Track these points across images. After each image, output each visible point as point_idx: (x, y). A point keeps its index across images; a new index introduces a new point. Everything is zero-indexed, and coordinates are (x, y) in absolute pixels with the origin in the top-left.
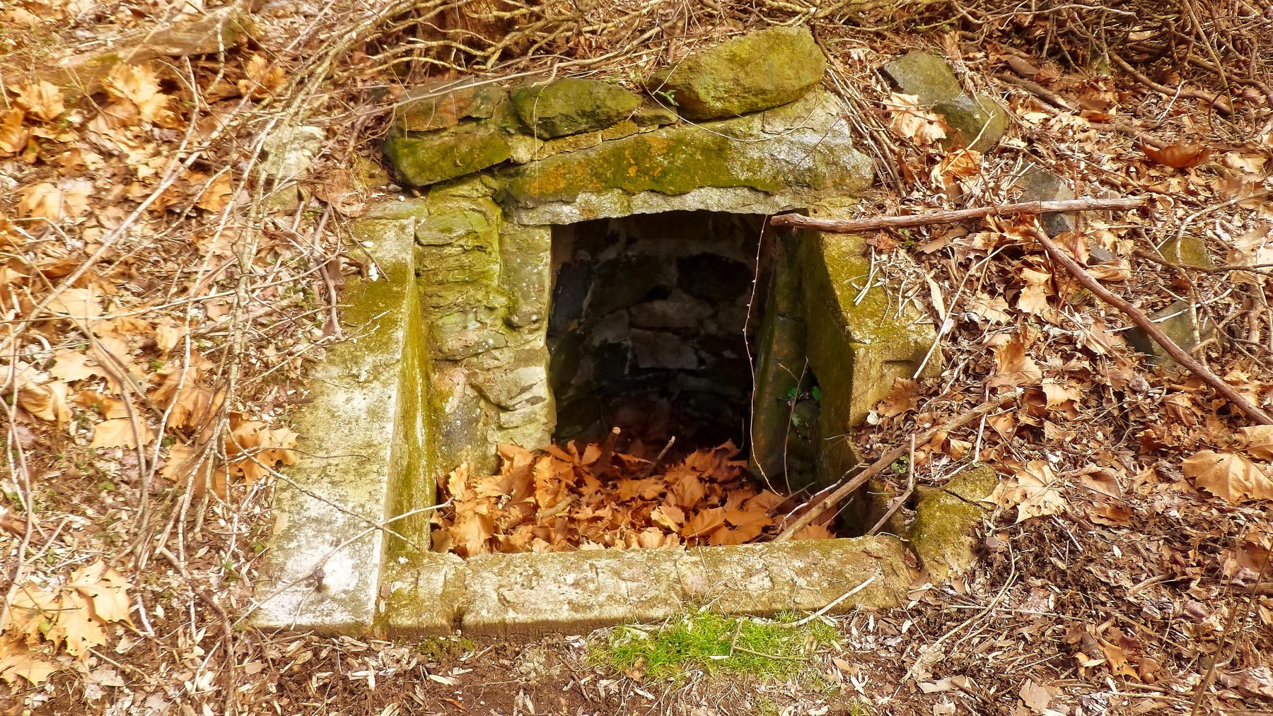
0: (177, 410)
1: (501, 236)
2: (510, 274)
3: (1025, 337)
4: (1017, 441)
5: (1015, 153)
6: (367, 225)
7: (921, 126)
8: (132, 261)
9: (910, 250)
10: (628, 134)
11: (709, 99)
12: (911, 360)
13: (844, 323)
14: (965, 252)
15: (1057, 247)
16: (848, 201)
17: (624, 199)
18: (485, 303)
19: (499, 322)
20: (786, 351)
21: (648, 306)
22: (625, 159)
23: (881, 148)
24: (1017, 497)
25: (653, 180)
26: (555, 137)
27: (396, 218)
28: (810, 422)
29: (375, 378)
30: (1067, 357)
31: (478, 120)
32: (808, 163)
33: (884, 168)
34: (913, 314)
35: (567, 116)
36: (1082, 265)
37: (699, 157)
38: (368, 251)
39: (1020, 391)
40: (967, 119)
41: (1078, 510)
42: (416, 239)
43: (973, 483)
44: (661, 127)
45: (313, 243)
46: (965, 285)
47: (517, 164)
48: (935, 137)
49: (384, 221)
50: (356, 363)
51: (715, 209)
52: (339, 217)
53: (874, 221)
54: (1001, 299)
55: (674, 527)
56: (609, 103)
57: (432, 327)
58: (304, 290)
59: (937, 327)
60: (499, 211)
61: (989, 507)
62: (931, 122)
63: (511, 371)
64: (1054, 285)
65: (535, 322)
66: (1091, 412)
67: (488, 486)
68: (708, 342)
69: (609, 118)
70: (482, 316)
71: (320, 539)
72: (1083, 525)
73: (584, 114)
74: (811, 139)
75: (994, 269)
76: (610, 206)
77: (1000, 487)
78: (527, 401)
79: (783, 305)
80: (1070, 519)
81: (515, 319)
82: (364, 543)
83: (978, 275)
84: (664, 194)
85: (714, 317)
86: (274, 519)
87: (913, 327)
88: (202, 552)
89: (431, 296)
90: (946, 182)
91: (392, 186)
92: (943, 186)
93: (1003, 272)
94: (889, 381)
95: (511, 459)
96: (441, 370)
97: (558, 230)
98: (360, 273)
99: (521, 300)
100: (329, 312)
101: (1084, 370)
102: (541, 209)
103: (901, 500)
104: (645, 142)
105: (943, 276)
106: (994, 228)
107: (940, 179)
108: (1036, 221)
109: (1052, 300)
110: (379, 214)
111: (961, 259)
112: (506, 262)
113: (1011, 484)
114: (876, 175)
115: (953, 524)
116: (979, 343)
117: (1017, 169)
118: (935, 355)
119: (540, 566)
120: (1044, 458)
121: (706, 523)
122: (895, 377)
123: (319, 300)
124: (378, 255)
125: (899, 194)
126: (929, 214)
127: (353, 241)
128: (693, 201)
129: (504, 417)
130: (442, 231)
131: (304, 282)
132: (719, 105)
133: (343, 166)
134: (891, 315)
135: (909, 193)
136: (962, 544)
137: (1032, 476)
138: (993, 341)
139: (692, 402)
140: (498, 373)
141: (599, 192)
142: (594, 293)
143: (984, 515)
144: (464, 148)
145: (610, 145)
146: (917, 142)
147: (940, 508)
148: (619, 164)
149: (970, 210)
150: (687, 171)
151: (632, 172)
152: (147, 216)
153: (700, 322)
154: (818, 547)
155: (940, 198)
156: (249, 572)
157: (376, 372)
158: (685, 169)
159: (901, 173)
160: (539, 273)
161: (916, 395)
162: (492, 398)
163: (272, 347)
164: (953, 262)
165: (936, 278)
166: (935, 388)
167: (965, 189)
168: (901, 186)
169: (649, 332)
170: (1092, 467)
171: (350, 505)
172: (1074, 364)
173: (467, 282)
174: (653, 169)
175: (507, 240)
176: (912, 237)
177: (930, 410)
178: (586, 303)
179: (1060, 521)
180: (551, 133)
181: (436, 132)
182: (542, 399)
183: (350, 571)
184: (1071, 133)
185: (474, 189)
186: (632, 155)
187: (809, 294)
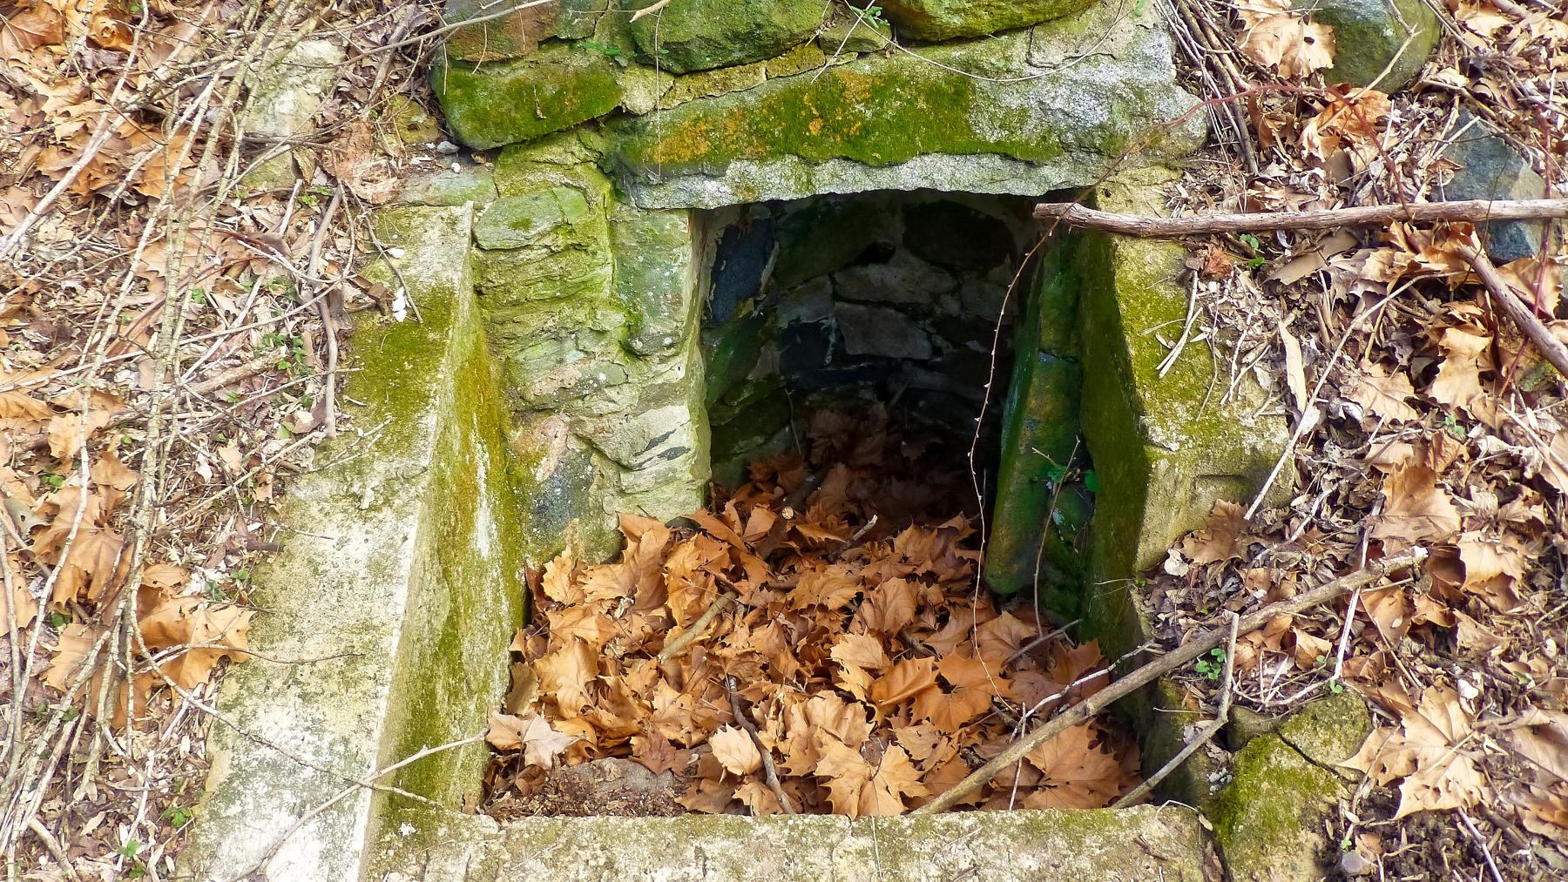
0: (67, 576)
1: (612, 225)
2: (630, 280)
3: (1438, 452)
4: (1409, 646)
5: (1448, 96)
6: (398, 217)
7: (1293, 45)
8: (33, 288)
9: (1256, 274)
10: (813, 70)
11: (941, 13)
12: (1247, 477)
13: (1138, 409)
14: (1350, 281)
15: (1504, 281)
16: (1162, 174)
17: (802, 170)
18: (590, 324)
19: (615, 349)
20: (1048, 408)
21: (860, 271)
22: (805, 107)
23: (1223, 85)
24: (1399, 766)
25: (850, 141)
26: (692, 72)
27: (444, 204)
28: (1079, 525)
29: (387, 502)
30: (1507, 494)
31: (571, 42)
32: (1099, 115)
33: (1225, 118)
34: (1255, 397)
35: (708, 41)
36: (1543, 316)
37: (921, 104)
38: (395, 263)
39: (1421, 553)
40: (1372, 36)
41: (1510, 801)
42: (474, 239)
43: (1329, 727)
44: (862, 55)
45: (314, 256)
46: (1345, 348)
47: (631, 115)
48: (1314, 65)
49: (425, 210)
50: (360, 473)
51: (946, 188)
52: (354, 204)
53: (1202, 218)
54: (1403, 378)
55: (859, 695)
56: (777, 19)
57: (507, 366)
58: (289, 343)
59: (1291, 421)
60: (607, 187)
61: (1352, 777)
62: (1309, 41)
63: (636, 415)
64: (1495, 354)
65: (669, 347)
66: (1539, 599)
67: (604, 583)
68: (945, 326)
69: (777, 43)
70: (586, 343)
71: (276, 801)
72: (1506, 827)
73: (736, 37)
74: (1110, 75)
75: (1394, 314)
76: (779, 181)
77: (1373, 740)
78: (661, 456)
79: (1049, 336)
80: (1489, 819)
81: (638, 345)
82: (341, 811)
83: (1367, 328)
84: (863, 163)
85: (956, 291)
86: (209, 762)
87: (1250, 422)
88: (93, 823)
89: (502, 323)
90: (1326, 145)
91: (445, 145)
92: (1321, 155)
93: (1410, 326)
94: (1205, 504)
95: (638, 539)
96: (527, 424)
97: (701, 218)
98: (377, 307)
99: (647, 317)
100: (325, 379)
101: (1534, 522)
102: (672, 186)
103: (1209, 727)
104: (836, 80)
105: (1306, 324)
106: (1401, 243)
107: (1317, 141)
108: (1474, 237)
109: (1488, 378)
110: (418, 197)
111: (1341, 293)
112: (621, 260)
113: (1394, 738)
114: (1211, 131)
115: (1288, 807)
116: (1361, 457)
117: (1448, 127)
118: (1285, 474)
119: (617, 850)
120: (1452, 683)
121: (910, 679)
122: (1212, 497)
123: (313, 359)
124: (412, 271)
125: (1246, 166)
126: (1293, 213)
127: (374, 247)
128: (910, 176)
129: (627, 479)
130: (515, 226)
131: (291, 325)
132: (957, 21)
133: (365, 113)
134: (1221, 398)
135: (1263, 165)
136: (1300, 846)
137: (1430, 725)
138: (1384, 457)
139: (921, 404)
140: (615, 421)
141: (762, 160)
142: (779, 256)
143: (1342, 792)
144: (550, 90)
145: (780, 86)
146: (1284, 73)
147: (1269, 774)
148: (794, 116)
149: (1366, 209)
150: (902, 128)
151: (814, 128)
152: (66, 204)
153: (936, 297)
154: (1065, 826)
155: (1314, 177)
156: (162, 862)
157: (388, 492)
158: (900, 124)
159: (1253, 130)
160: (674, 278)
161: (1242, 536)
162: (607, 452)
163: (232, 443)
164: (1326, 298)
165: (1296, 327)
166: (1280, 525)
167: (1357, 163)
168: (1251, 152)
169: (862, 308)
170: (1535, 716)
171: (328, 738)
172: (1517, 510)
173: (559, 298)
174: (849, 124)
175: (622, 229)
176: (1262, 250)
177: (1266, 563)
178: (765, 275)
179: (1471, 821)
180: (685, 65)
181: (505, 62)
182: (683, 450)
183: (316, 861)
184: (1544, 54)
185: (570, 152)
186: (813, 100)
187: (1089, 325)
